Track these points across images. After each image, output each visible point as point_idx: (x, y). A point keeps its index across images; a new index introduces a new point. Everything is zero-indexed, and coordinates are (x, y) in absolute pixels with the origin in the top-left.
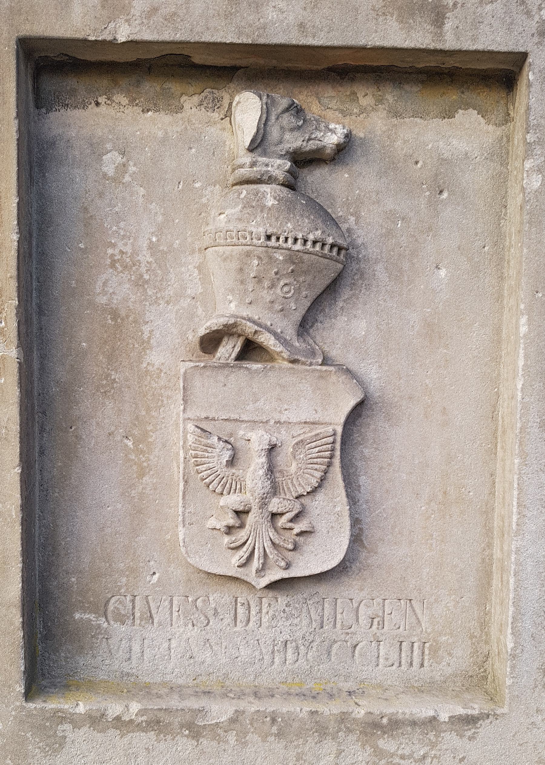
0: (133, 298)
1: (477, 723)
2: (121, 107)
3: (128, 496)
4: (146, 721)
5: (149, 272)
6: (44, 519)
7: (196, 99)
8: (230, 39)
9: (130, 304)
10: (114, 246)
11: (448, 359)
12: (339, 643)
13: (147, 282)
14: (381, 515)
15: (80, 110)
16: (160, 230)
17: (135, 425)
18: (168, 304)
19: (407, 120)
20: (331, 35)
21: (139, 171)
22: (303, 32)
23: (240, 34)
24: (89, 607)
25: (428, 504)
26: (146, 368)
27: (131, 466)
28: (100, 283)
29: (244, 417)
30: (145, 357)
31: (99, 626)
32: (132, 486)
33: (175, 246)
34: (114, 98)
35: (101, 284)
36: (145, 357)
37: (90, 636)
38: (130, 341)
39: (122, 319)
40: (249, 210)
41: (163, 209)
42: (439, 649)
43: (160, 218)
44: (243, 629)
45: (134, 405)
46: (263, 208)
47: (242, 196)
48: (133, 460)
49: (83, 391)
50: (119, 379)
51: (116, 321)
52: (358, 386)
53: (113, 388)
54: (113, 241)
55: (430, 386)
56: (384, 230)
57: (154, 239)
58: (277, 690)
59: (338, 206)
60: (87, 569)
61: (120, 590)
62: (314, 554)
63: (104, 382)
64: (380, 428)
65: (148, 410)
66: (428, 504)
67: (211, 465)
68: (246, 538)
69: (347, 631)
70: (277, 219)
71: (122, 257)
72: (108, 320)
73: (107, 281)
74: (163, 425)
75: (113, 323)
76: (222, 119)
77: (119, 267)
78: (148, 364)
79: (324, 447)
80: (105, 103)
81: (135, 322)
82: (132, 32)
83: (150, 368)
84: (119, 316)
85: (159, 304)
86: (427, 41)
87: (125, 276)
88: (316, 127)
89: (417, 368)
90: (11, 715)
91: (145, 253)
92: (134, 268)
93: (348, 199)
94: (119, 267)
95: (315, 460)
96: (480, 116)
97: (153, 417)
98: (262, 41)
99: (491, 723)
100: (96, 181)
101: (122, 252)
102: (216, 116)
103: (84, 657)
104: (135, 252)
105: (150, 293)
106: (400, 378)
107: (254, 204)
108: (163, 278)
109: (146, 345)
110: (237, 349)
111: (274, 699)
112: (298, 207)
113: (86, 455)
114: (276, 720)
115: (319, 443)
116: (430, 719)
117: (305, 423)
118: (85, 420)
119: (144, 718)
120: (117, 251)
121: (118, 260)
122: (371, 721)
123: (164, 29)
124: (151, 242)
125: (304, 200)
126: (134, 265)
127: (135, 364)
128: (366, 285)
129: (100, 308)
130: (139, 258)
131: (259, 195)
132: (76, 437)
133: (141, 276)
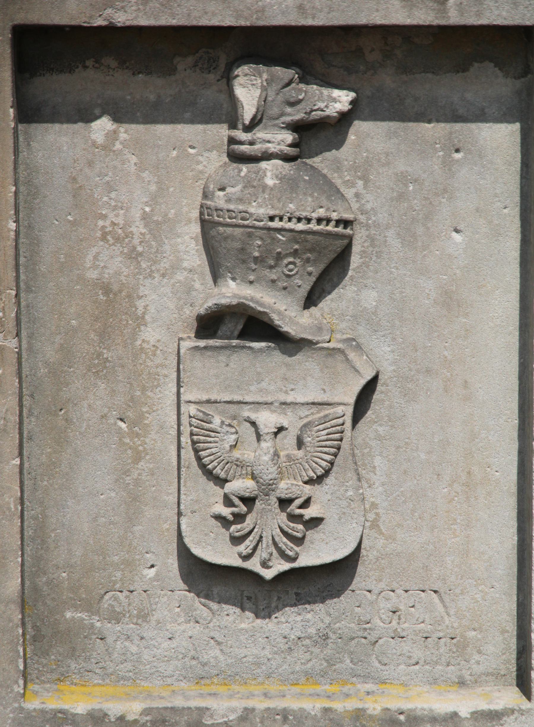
0: (125, 271)
1: (500, 719)
2: (111, 70)
3: (123, 483)
4: (151, 721)
5: (143, 244)
6: (32, 510)
7: (190, 60)
8: (228, 21)
9: (123, 278)
10: (104, 217)
11: (468, 328)
12: (356, 640)
13: (141, 254)
14: (399, 498)
15: (67, 74)
16: (154, 200)
17: (129, 406)
18: (164, 277)
19: (417, 76)
20: (330, 16)
21: (131, 138)
22: (303, 13)
23: (238, 17)
24: (80, 605)
25: (450, 485)
26: (141, 345)
27: (126, 450)
28: (90, 257)
29: (248, 399)
30: (140, 333)
31: (92, 626)
32: (127, 473)
33: (170, 216)
34: (103, 61)
35: (92, 258)
36: (140, 333)
37: (82, 636)
38: (123, 317)
39: (115, 294)
40: (251, 190)
41: (157, 177)
42: (468, 646)
43: (153, 188)
44: (250, 625)
45: (128, 385)
46: (265, 187)
47: (243, 174)
48: (129, 444)
49: (73, 371)
50: (112, 357)
51: (108, 297)
52: (369, 363)
53: (105, 367)
54: (104, 213)
55: (449, 357)
56: (395, 194)
57: (147, 209)
58: (288, 691)
59: (344, 170)
60: (79, 563)
61: (114, 585)
62: (325, 542)
63: (96, 361)
64: (395, 404)
65: (144, 389)
66: (450, 485)
67: (214, 450)
68: (252, 527)
69: (365, 626)
70: (279, 200)
71: (113, 228)
72: (99, 295)
73: (98, 253)
74: (160, 406)
75: (105, 298)
76: (218, 80)
77: (110, 239)
78: (143, 341)
79: (334, 429)
80: (93, 66)
81: (129, 296)
82: (128, 18)
83: (145, 345)
84: (112, 291)
85: (154, 278)
86: (430, 18)
87: (117, 249)
88: (319, 97)
89: (434, 339)
90: (9, 718)
91: (137, 223)
92: (126, 240)
93: (355, 162)
94: (110, 239)
95: (324, 443)
96: (497, 69)
97: (149, 397)
98: (261, 23)
99: (516, 719)
100: (84, 150)
101: (113, 224)
102: (212, 77)
103: (76, 659)
104: (128, 223)
105: (144, 265)
106: (416, 351)
107: (255, 184)
108: (157, 249)
109: (140, 321)
110: (240, 327)
111: (285, 699)
112: (302, 185)
113: (77, 439)
114: (288, 718)
115: (328, 425)
116: (451, 715)
117: (313, 404)
118: (75, 402)
119: (148, 718)
120: (108, 223)
121: (110, 232)
122: (388, 718)
123: (160, 14)
124: (145, 212)
125: (306, 175)
126: (127, 237)
127: (128, 341)
128: (376, 253)
129: (90, 282)
130: (131, 229)
131: (260, 174)
132: (66, 420)
133: (134, 248)
